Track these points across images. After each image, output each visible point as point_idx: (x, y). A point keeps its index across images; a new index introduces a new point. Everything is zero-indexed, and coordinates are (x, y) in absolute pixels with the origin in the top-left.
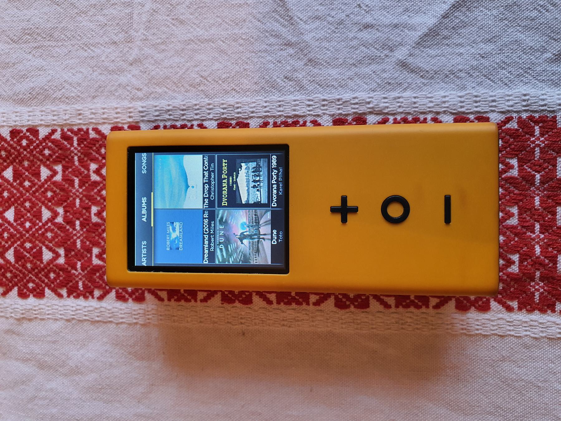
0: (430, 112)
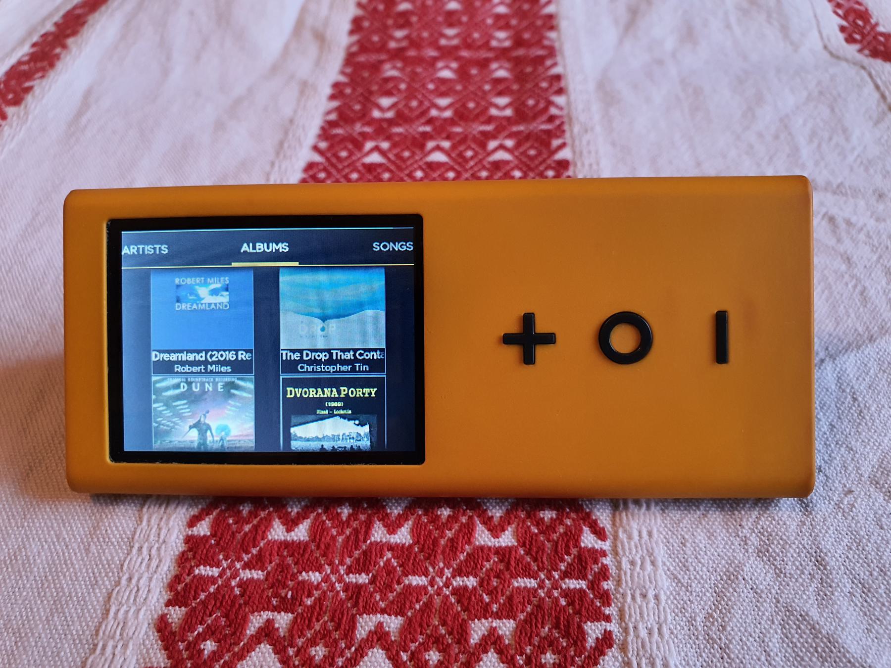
0: (626, 630)
